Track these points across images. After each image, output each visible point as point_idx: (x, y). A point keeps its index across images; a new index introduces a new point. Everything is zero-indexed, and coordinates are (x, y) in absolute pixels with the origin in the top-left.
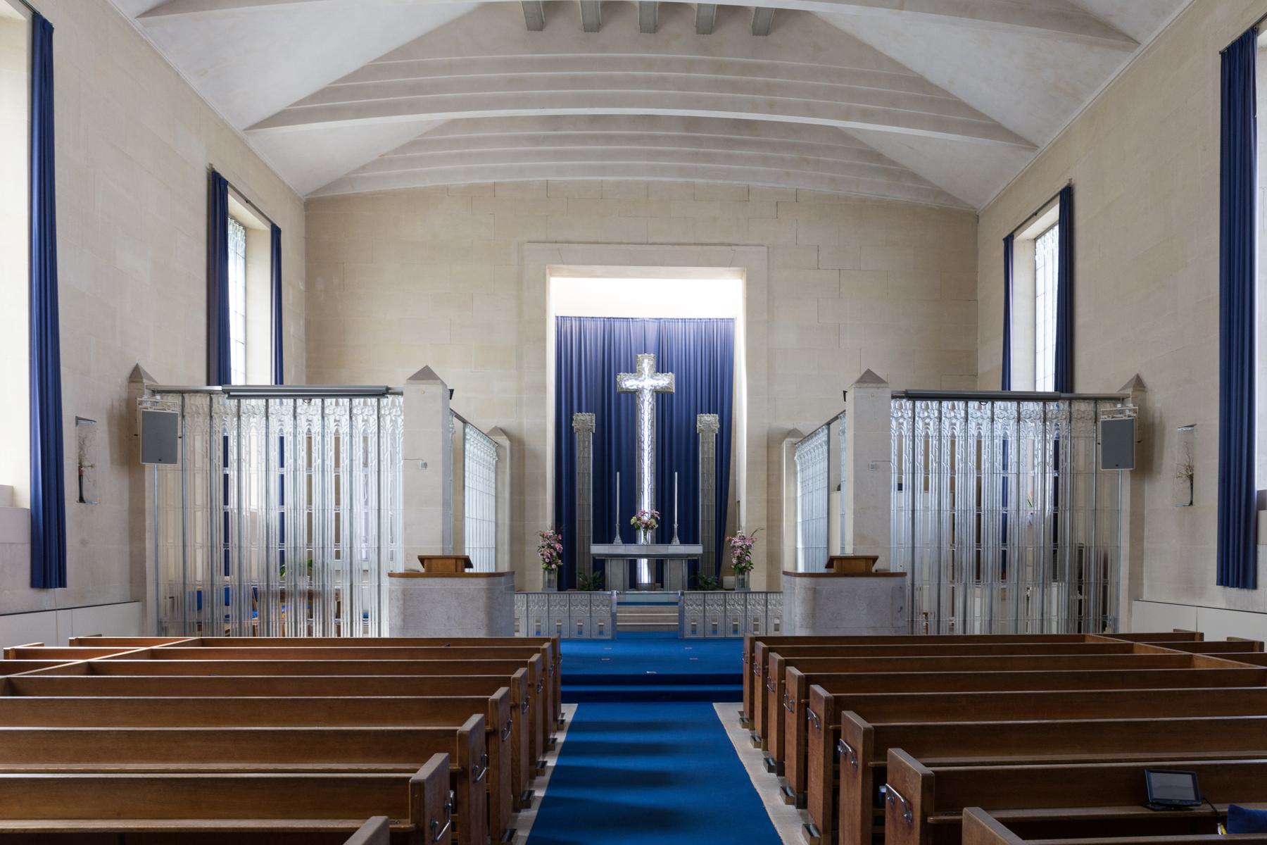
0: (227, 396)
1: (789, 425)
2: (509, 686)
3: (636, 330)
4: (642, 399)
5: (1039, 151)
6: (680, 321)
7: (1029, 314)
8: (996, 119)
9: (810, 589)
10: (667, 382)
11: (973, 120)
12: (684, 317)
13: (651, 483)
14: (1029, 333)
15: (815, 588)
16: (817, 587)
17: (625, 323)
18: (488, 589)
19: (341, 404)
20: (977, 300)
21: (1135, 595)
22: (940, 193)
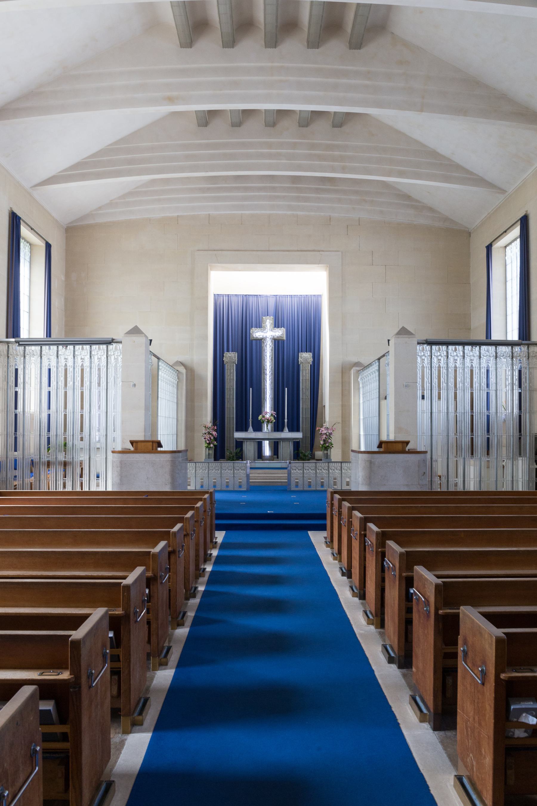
0: (17, 344)
1: (355, 359)
3: (262, 302)
4: (265, 344)
5: (507, 194)
6: (289, 296)
8: (480, 175)
9: (367, 461)
10: (281, 334)
13: (271, 395)
14: (503, 303)
16: (372, 460)
17: (256, 298)
18: (171, 460)
20: (470, 284)
22: (446, 219)
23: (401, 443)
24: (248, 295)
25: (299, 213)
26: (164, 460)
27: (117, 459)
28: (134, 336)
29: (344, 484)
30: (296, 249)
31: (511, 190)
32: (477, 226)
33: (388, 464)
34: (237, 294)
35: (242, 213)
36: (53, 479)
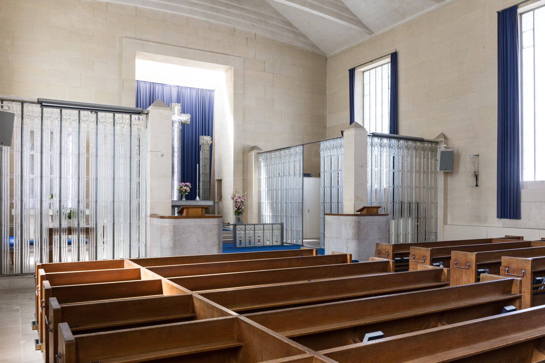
0: (40, 105)
1: (252, 144)
2: (490, 270)
3: (166, 90)
5: (373, 35)
6: (188, 88)
7: (361, 103)
8: (360, 18)
9: (357, 221)
10: (187, 119)
11: (352, 17)
12: (190, 87)
14: (361, 111)
15: (359, 221)
16: (360, 221)
17: (161, 86)
18: (218, 224)
19: (141, 119)
20: (326, 95)
21: (445, 223)
22: (313, 45)
23: (376, 208)
24: (155, 83)
25: (212, 21)
26: (212, 224)
27: (169, 224)
28: (162, 109)
29: (257, 240)
30: (208, 50)
31: (378, 33)
32: (335, 54)
33: (369, 224)
34: (145, 81)
35: (165, 12)
36: (18, 248)
